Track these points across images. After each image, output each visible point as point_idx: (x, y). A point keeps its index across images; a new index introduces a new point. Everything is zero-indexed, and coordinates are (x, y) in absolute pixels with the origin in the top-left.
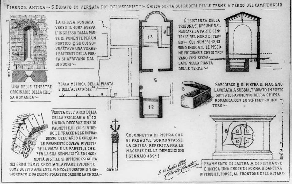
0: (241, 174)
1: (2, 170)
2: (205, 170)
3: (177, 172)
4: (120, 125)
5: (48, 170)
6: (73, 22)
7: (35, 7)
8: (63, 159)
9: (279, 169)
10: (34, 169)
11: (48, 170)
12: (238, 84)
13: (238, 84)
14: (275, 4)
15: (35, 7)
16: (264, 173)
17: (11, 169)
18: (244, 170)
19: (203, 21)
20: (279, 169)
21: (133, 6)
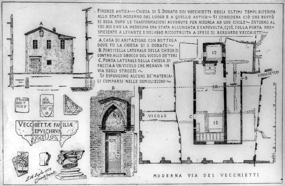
0: (98, 66)
1: (64, 86)
2: (246, 176)
3: (49, 169)
4: (82, 9)
5: (114, 33)
6: (147, 11)
7: (121, 11)
8: (154, 11)
9: (170, 12)
10: (112, 56)
11: (114, 33)
12: (159, 10)
13: (159, 10)
14: (222, 11)
15: (121, 11)
16: (151, 32)
17: (99, 55)
18: (204, 176)
19: (109, 11)
20: (170, 12)
21: (202, 11)
